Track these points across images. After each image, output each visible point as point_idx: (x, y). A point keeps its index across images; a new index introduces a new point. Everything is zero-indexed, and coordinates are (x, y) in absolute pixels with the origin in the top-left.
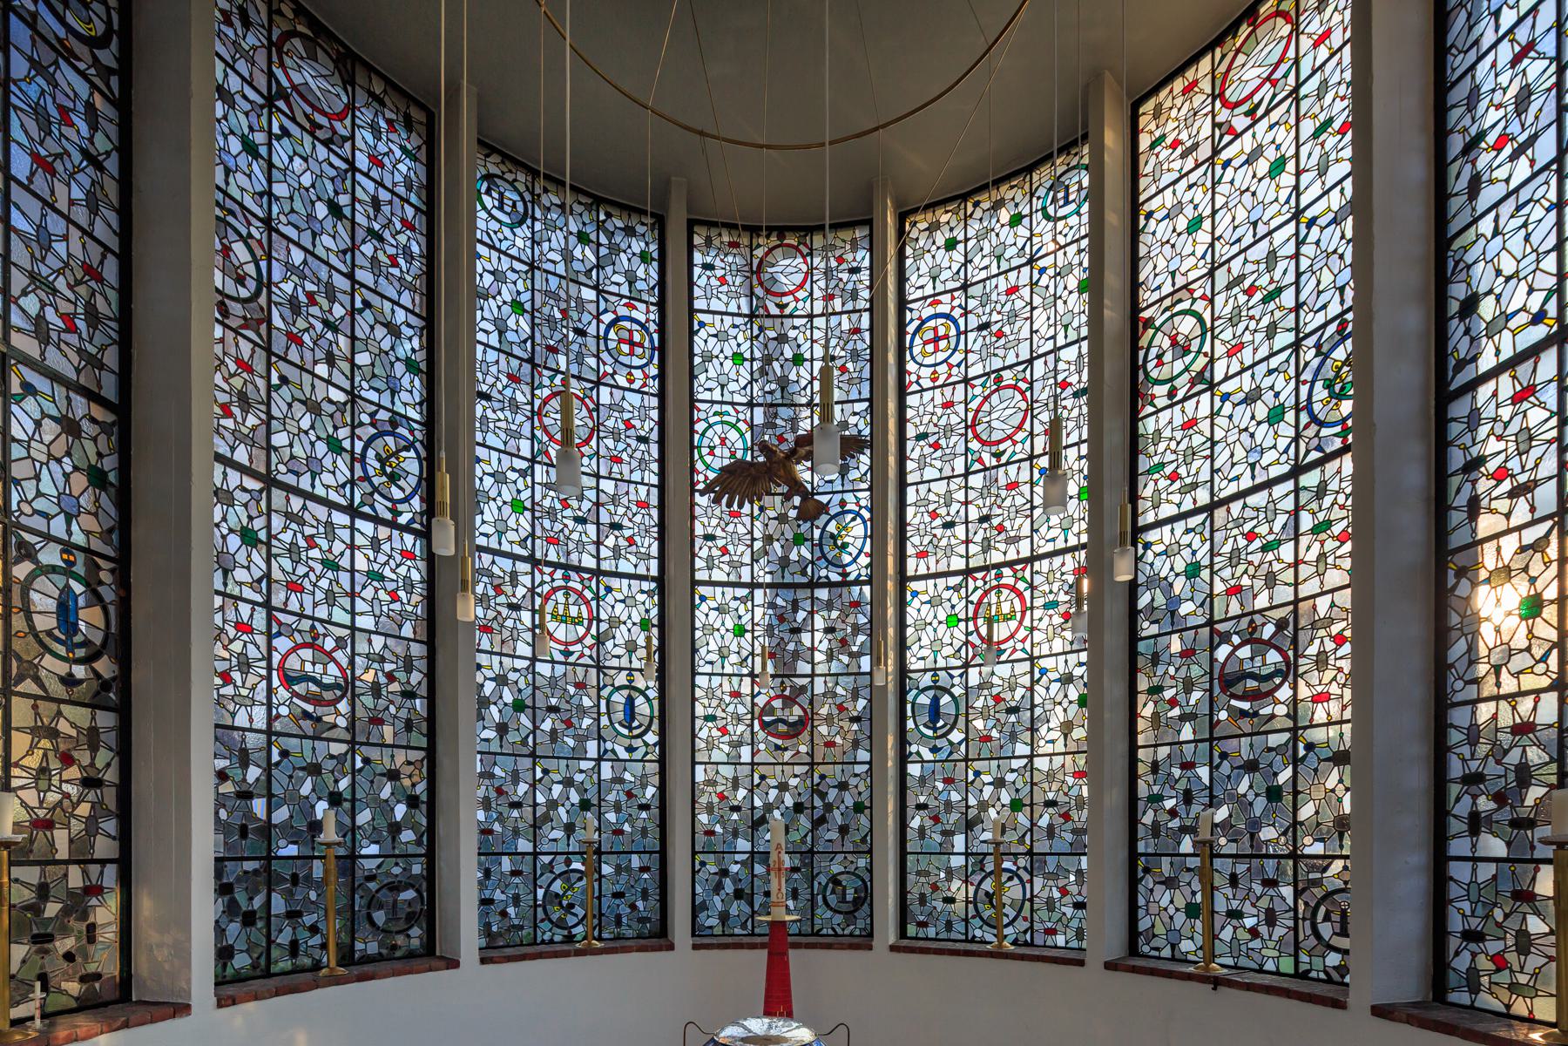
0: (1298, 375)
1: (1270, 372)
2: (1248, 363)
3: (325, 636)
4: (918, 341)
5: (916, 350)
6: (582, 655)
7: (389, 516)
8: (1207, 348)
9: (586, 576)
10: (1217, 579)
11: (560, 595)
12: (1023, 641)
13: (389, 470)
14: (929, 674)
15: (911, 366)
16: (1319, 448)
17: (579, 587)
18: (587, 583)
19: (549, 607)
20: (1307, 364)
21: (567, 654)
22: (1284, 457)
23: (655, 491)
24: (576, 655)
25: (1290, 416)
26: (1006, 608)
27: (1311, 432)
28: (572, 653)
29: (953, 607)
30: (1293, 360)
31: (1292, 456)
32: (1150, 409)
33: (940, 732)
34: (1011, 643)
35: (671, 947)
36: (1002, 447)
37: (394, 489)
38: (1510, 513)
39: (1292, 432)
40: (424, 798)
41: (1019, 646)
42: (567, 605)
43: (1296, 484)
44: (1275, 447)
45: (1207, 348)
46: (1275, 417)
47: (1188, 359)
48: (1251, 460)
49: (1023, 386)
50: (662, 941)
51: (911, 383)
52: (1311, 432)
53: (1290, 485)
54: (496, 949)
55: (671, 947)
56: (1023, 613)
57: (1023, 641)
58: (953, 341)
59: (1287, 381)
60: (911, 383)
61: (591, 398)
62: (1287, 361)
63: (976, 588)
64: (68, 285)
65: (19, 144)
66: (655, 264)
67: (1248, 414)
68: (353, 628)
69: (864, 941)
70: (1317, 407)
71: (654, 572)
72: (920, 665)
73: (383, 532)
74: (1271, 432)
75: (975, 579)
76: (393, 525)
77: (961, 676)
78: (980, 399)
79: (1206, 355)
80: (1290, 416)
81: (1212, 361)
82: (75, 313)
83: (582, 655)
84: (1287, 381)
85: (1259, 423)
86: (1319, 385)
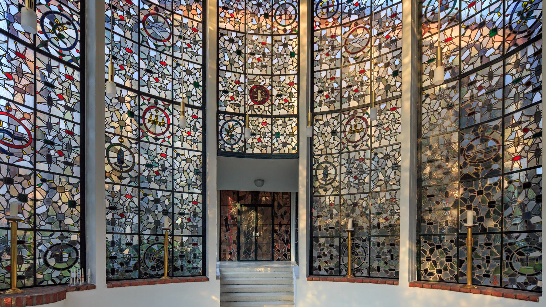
0: (504, 12)
1: (491, 13)
2: (479, 9)
3: (16, 110)
4: (319, 7)
5: (318, 11)
6: (164, 141)
7: (57, 55)
8: (457, 6)
9: (167, 103)
10: (369, 165)
11: (153, 110)
12: (367, 141)
13: (57, 32)
14: (323, 157)
15: (316, 19)
16: (515, 44)
17: (163, 108)
18: (167, 107)
19: (148, 115)
20: (509, 6)
21: (156, 139)
22: (498, 51)
23: (201, 196)
24: (161, 140)
25: (500, 32)
26: (359, 127)
27: (511, 38)
28: (159, 139)
29: (335, 126)
30: (502, 7)
31: (502, 50)
32: (427, 34)
33: (328, 182)
34: (361, 142)
35: (208, 280)
36: (358, 55)
37: (60, 42)
38: (522, 116)
39: (501, 39)
40: (79, 202)
41: (365, 143)
42: (156, 116)
43: (504, 63)
44: (493, 47)
45: (457, 6)
46: (494, 32)
47: (447, 11)
48: (480, 55)
49: (368, 27)
50: (203, 277)
51: (316, 26)
52: (511, 38)
53: (501, 63)
54: (113, 278)
55: (208, 280)
56: (367, 128)
57: (367, 141)
58: (335, 7)
59: (499, 17)
60: (316, 26)
61: (170, 19)
62: (499, 7)
63: (345, 118)
64: (7, 61)
65: (31, 61)
66: (201, 88)
67: (479, 33)
68: (35, 110)
69: (393, 277)
70: (514, 26)
71: (200, 148)
72: (319, 152)
73: (54, 63)
74: (491, 40)
75: (344, 114)
76: (60, 60)
77: (337, 157)
78: (348, 33)
79: (457, 9)
80: (500, 32)
81: (460, 11)
82: (12, 72)
83: (164, 141)
84: (499, 17)
85: (485, 37)
86: (515, 15)
